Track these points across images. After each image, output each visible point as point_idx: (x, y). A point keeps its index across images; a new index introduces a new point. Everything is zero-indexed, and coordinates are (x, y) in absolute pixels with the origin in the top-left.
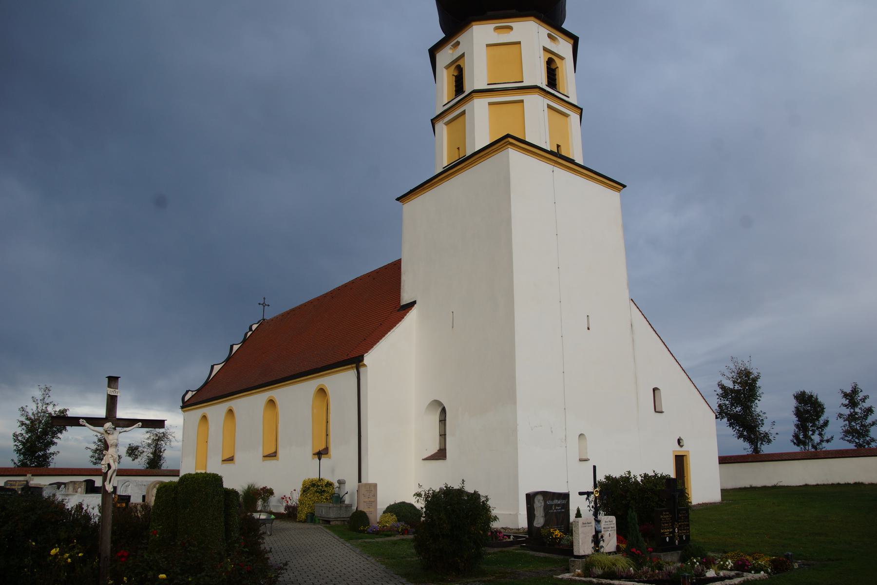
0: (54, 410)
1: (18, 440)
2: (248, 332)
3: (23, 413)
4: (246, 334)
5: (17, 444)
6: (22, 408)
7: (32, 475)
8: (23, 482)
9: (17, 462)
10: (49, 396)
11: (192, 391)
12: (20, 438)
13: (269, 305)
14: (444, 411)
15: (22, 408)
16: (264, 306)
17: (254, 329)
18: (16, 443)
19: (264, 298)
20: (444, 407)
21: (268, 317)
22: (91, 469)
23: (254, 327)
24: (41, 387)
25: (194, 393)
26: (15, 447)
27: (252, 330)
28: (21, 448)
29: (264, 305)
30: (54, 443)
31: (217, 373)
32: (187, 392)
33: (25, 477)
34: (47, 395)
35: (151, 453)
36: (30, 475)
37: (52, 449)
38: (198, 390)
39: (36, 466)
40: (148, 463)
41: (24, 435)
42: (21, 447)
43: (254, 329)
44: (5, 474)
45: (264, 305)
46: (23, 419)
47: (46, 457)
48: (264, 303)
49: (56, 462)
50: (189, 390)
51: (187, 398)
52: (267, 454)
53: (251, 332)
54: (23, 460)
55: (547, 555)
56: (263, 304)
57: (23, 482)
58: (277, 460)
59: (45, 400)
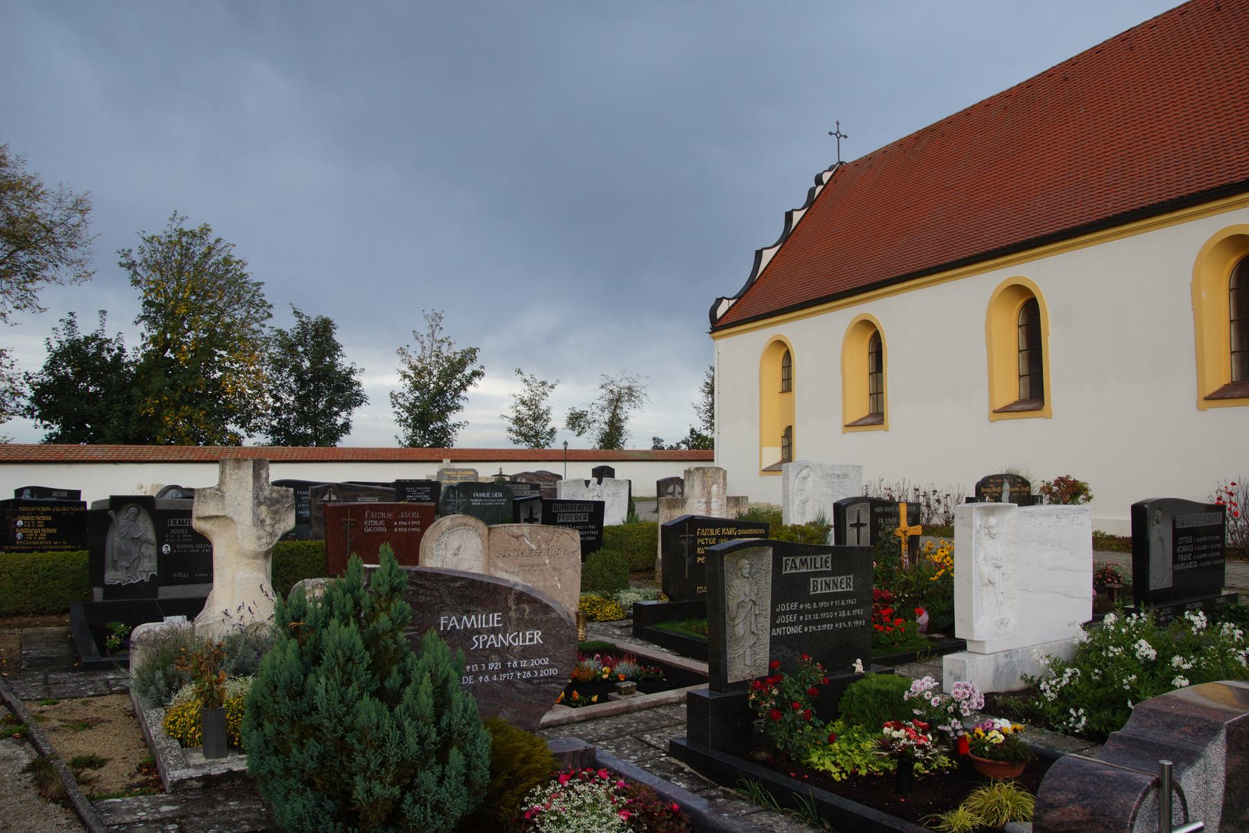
0: (452, 351)
1: (399, 404)
2: (816, 188)
3: (404, 357)
4: (812, 191)
5: (398, 411)
6: (401, 349)
7: (452, 461)
8: (468, 473)
9: (403, 441)
10: (441, 328)
11: (729, 299)
12: (400, 400)
13: (831, 134)
14: (788, 356)
15: (401, 349)
16: (838, 138)
17: (825, 180)
18: (396, 409)
19: (838, 123)
20: (788, 350)
21: (849, 157)
22: (513, 450)
23: (826, 177)
24: (426, 313)
25: (732, 302)
26: (396, 415)
27: (822, 183)
28: (405, 417)
29: (838, 135)
30: (458, 408)
31: (771, 261)
32: (719, 301)
33: (441, 464)
34: (438, 327)
35: (606, 423)
36: (449, 460)
37: (453, 418)
38: (739, 297)
39: (431, 446)
40: (602, 441)
41: (406, 395)
42: (405, 415)
43: (825, 180)
44: (403, 459)
45: (838, 135)
46: (405, 368)
47: (444, 431)
48: (838, 132)
49: (461, 440)
50: (724, 298)
51: (721, 311)
52: (853, 421)
53: (819, 188)
54: (413, 436)
55: (697, 773)
56: (836, 134)
57: (468, 473)
58: (1049, 417)
59: (436, 334)
